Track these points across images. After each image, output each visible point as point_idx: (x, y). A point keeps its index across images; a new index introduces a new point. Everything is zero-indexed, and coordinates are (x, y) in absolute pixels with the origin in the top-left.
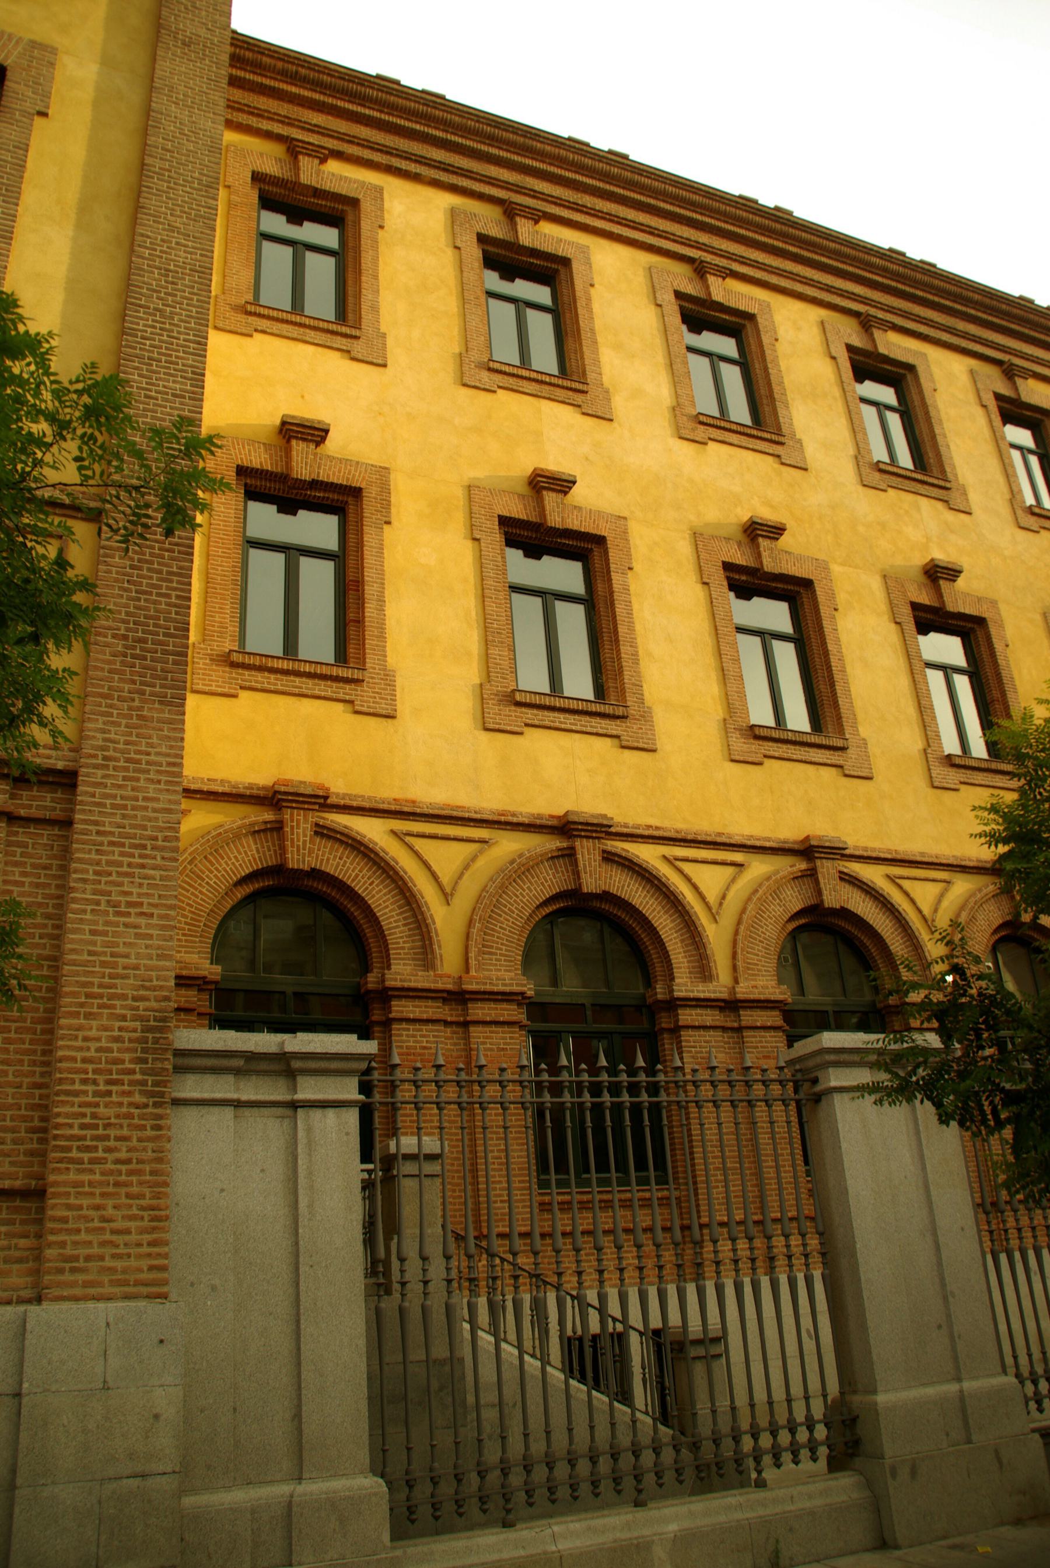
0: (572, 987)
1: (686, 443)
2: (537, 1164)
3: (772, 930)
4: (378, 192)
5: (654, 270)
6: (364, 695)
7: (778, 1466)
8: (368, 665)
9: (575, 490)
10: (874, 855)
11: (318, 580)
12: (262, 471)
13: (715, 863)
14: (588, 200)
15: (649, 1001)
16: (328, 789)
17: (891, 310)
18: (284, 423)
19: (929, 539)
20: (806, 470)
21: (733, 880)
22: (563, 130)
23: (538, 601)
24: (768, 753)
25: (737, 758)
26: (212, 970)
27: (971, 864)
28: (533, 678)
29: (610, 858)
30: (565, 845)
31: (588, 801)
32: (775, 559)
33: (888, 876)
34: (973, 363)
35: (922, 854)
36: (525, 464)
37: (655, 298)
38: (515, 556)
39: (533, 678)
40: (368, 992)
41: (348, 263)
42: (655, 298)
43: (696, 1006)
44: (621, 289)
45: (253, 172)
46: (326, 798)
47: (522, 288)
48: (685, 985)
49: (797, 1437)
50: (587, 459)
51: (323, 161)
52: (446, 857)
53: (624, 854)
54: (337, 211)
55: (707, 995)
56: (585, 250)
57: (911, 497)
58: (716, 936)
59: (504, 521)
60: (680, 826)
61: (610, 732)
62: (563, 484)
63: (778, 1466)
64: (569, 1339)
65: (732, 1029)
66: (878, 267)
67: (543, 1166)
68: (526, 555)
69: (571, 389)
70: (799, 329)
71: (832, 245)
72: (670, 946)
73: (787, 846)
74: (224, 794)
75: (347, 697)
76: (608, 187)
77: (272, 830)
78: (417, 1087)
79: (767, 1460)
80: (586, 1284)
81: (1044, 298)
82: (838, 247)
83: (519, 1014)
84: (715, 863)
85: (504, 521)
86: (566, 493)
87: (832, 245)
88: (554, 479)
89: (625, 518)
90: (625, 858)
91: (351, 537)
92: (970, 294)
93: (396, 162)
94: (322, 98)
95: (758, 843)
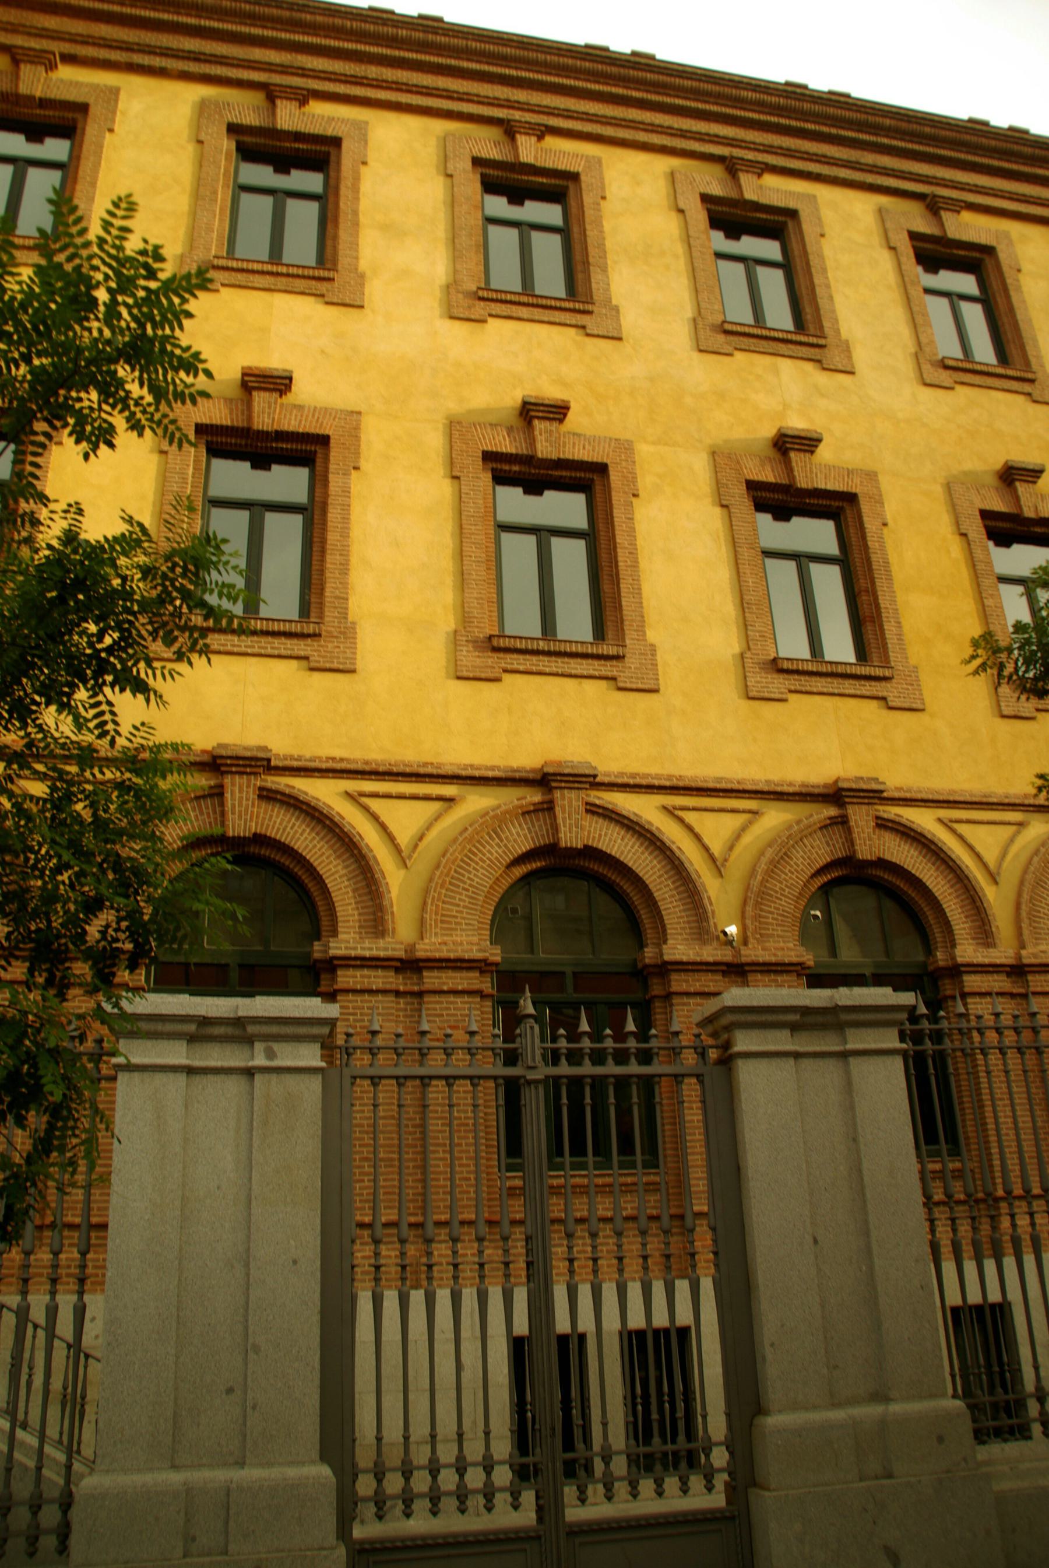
0: (549, 953)
1: (457, 323)
3: (488, 874)
5: (677, 176)
8: (628, 642)
9: (570, 415)
10: (644, 782)
11: (570, 559)
12: (212, 426)
13: (415, 797)
14: (373, 71)
15: (931, 968)
16: (595, 768)
17: (769, 149)
19: (786, 406)
20: (620, 339)
21: (437, 818)
22: (365, 5)
23: (791, 565)
24: (509, 667)
25: (465, 674)
27: (791, 790)
28: (793, 645)
29: (883, 824)
30: (212, 783)
31: (573, 751)
32: (814, 473)
33: (665, 808)
34: (675, 162)
35: (719, 780)
37: (446, 168)
38: (765, 519)
39: (793, 645)
40: (646, 966)
42: (446, 168)
43: (362, 967)
44: (852, 234)
46: (595, 776)
47: (535, 211)
48: (967, 951)
50: (323, 352)
53: (897, 819)
54: (319, 154)
55: (375, 953)
56: (813, 199)
57: (767, 360)
58: (397, 883)
59: (752, 486)
60: (338, 753)
61: (296, 653)
62: (809, 443)
64: (955, 1310)
65: (412, 994)
66: (751, 102)
68: (254, 467)
69: (314, 278)
70: (638, 184)
71: (688, 83)
72: (336, 896)
73: (517, 775)
74: (794, 794)
76: (397, 53)
77: (211, 795)
80: (383, 1282)
81: (1046, 125)
82: (695, 84)
83: (487, 984)
84: (415, 797)
85: (489, 457)
86: (812, 452)
87: (688, 83)
88: (265, 376)
89: (359, 413)
90: (290, 796)
91: (600, 515)
92: (879, 120)
93: (138, 59)
95: (477, 773)
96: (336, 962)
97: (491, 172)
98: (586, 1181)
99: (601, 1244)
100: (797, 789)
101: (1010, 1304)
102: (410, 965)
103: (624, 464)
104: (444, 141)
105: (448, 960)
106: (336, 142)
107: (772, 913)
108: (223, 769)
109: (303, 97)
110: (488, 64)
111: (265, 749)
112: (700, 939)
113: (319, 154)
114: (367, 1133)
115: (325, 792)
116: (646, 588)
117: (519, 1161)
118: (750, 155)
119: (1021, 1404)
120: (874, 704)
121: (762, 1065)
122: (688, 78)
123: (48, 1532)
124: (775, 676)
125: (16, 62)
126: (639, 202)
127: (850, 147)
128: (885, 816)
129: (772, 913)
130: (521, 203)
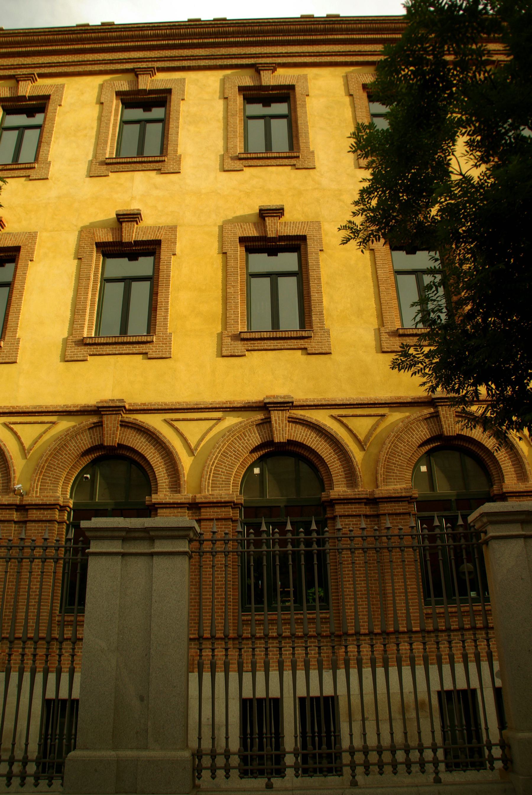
0: (273, 495)
2: (424, 592)
4: (305, 77)
6: (312, 345)
7: (381, 774)
11: (288, 287)
15: (492, 494)
18: (260, 210)
19: (133, 198)
22: (296, 14)
24: (250, 348)
26: (241, 499)
31: (279, 390)
36: (251, 208)
38: (400, 255)
41: (292, 120)
45: (239, 87)
49: (410, 756)
51: (274, 70)
52: (29, 432)
54: (286, 94)
63: (381, 774)
66: (151, 36)
67: (427, 594)
68: (130, 260)
75: (303, 346)
78: (213, 556)
79: (360, 770)
94: (82, 46)
96: (156, 506)
97: (5, 104)
98: (302, 616)
99: (415, 649)
100: (78, 408)
101: (338, 696)
102: (373, 501)
103: (30, 245)
104: (223, 81)
105: (213, 503)
106: (292, 88)
107: (49, 477)
108: (102, 413)
109: (273, 68)
110: (11, 48)
111: (289, 397)
112: (6, 492)
113: (286, 94)
114: (364, 587)
115: (154, 422)
116: (24, 308)
117: (82, 607)
118: (144, 65)
119: (338, 756)
120: (299, 352)
121: (103, 560)
122: (115, 32)
123: (30, 776)
124: (83, 347)
125: (258, 72)
126: (203, 100)
127: (212, 47)
128: (127, 420)
129: (49, 477)
130: (33, 116)
